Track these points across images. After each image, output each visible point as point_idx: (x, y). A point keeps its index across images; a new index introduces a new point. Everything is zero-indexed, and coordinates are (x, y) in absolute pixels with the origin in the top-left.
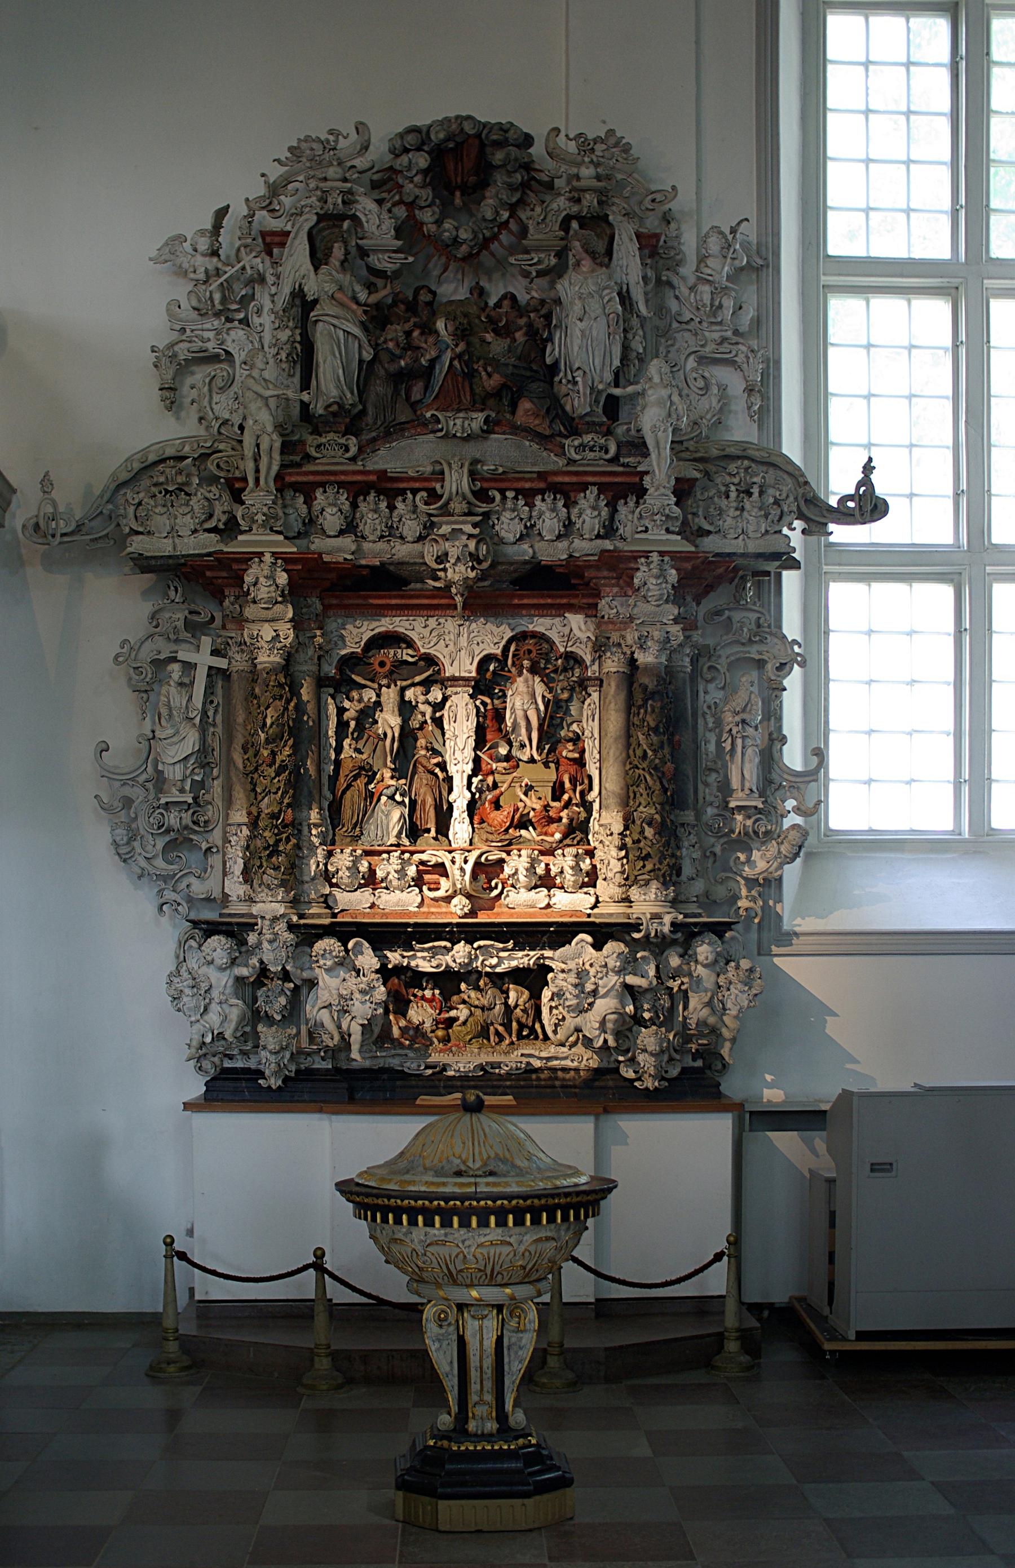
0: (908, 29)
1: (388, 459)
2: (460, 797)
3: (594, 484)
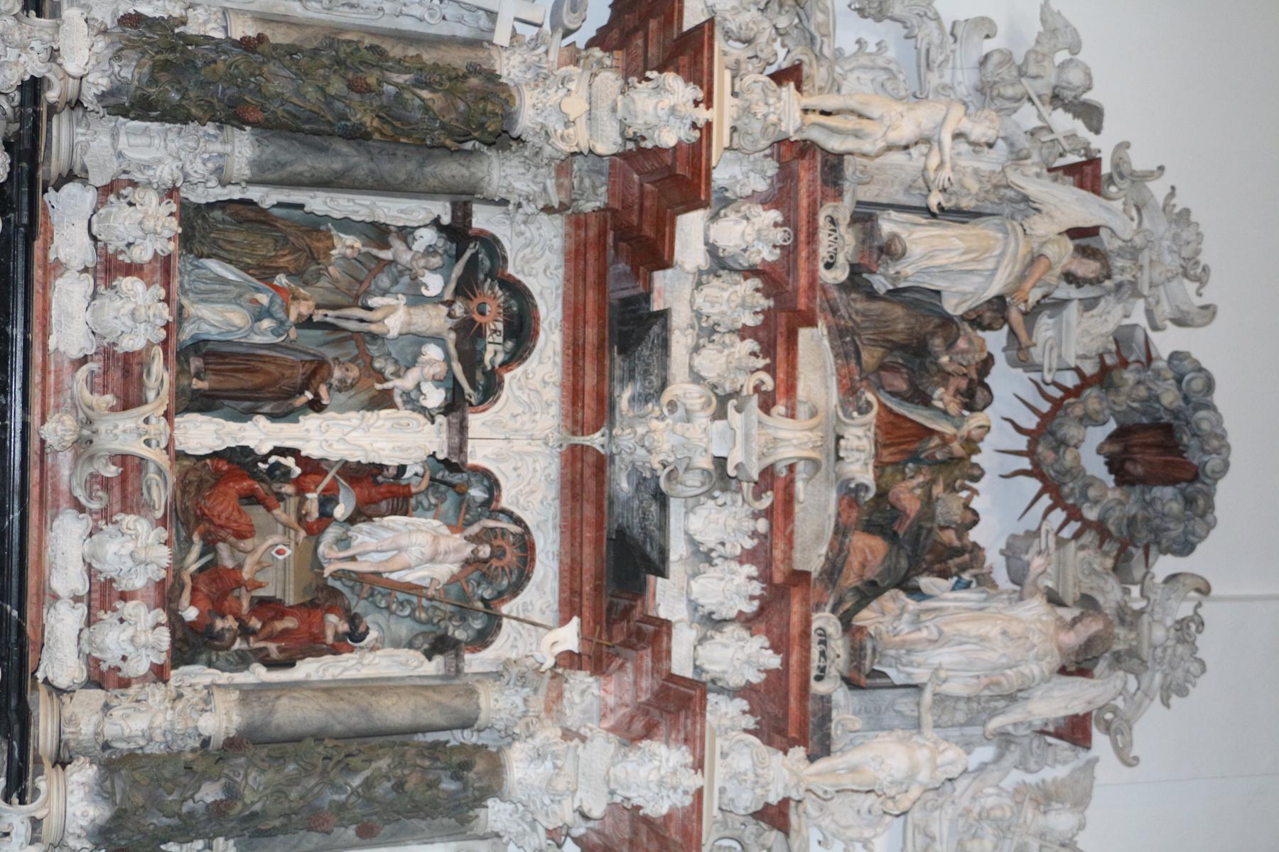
1: (814, 344)
2: (260, 434)
3: (786, 663)
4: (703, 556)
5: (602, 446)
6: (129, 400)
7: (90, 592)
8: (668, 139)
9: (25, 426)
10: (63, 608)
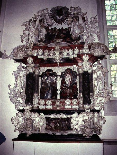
0: (110, 2)
1: (49, 45)
2: (59, 92)
4: (68, 54)
8: (32, 60)
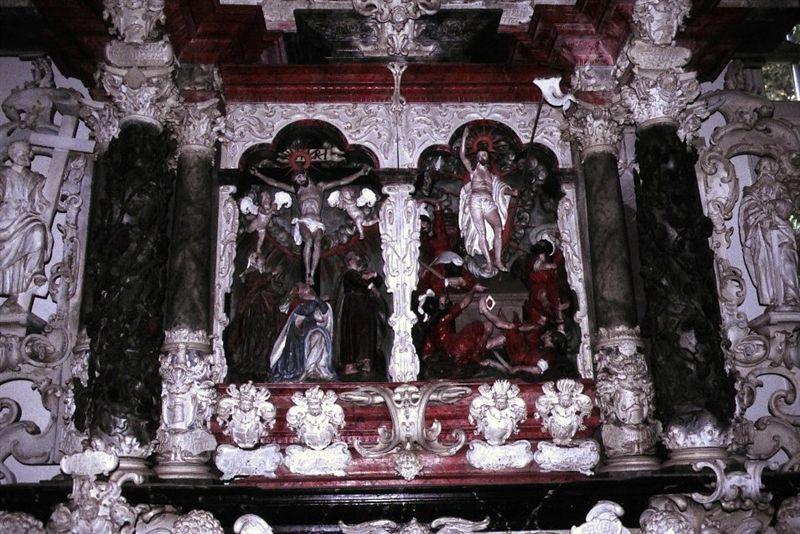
2: (402, 322)
5: (401, 67)
6: (384, 416)
7: (528, 439)
9: (407, 490)
10: (539, 458)
